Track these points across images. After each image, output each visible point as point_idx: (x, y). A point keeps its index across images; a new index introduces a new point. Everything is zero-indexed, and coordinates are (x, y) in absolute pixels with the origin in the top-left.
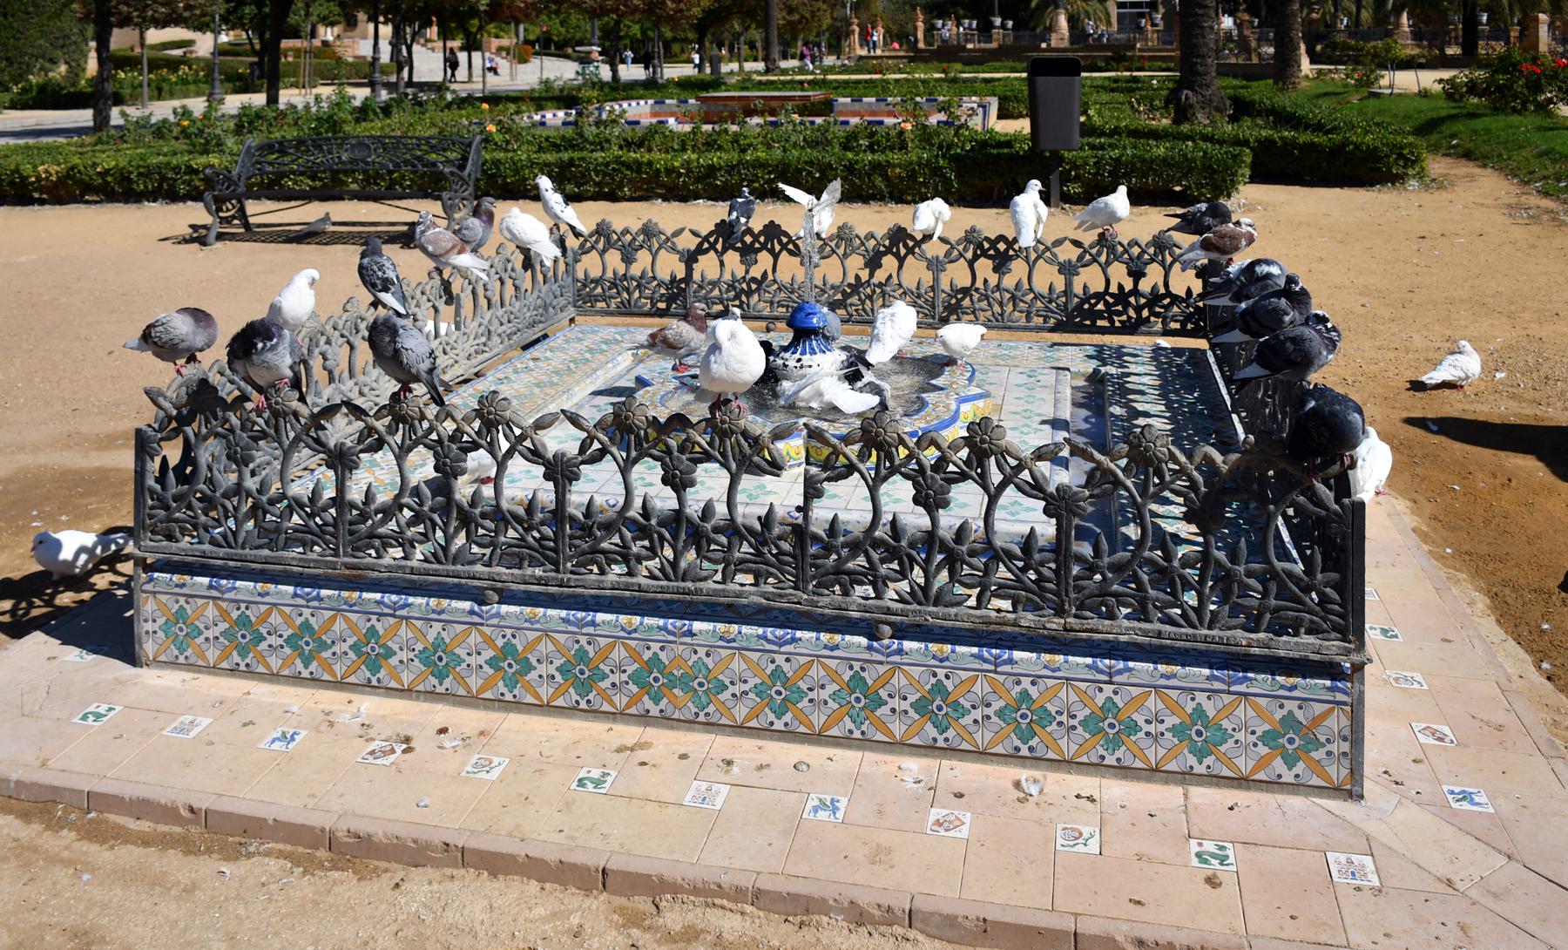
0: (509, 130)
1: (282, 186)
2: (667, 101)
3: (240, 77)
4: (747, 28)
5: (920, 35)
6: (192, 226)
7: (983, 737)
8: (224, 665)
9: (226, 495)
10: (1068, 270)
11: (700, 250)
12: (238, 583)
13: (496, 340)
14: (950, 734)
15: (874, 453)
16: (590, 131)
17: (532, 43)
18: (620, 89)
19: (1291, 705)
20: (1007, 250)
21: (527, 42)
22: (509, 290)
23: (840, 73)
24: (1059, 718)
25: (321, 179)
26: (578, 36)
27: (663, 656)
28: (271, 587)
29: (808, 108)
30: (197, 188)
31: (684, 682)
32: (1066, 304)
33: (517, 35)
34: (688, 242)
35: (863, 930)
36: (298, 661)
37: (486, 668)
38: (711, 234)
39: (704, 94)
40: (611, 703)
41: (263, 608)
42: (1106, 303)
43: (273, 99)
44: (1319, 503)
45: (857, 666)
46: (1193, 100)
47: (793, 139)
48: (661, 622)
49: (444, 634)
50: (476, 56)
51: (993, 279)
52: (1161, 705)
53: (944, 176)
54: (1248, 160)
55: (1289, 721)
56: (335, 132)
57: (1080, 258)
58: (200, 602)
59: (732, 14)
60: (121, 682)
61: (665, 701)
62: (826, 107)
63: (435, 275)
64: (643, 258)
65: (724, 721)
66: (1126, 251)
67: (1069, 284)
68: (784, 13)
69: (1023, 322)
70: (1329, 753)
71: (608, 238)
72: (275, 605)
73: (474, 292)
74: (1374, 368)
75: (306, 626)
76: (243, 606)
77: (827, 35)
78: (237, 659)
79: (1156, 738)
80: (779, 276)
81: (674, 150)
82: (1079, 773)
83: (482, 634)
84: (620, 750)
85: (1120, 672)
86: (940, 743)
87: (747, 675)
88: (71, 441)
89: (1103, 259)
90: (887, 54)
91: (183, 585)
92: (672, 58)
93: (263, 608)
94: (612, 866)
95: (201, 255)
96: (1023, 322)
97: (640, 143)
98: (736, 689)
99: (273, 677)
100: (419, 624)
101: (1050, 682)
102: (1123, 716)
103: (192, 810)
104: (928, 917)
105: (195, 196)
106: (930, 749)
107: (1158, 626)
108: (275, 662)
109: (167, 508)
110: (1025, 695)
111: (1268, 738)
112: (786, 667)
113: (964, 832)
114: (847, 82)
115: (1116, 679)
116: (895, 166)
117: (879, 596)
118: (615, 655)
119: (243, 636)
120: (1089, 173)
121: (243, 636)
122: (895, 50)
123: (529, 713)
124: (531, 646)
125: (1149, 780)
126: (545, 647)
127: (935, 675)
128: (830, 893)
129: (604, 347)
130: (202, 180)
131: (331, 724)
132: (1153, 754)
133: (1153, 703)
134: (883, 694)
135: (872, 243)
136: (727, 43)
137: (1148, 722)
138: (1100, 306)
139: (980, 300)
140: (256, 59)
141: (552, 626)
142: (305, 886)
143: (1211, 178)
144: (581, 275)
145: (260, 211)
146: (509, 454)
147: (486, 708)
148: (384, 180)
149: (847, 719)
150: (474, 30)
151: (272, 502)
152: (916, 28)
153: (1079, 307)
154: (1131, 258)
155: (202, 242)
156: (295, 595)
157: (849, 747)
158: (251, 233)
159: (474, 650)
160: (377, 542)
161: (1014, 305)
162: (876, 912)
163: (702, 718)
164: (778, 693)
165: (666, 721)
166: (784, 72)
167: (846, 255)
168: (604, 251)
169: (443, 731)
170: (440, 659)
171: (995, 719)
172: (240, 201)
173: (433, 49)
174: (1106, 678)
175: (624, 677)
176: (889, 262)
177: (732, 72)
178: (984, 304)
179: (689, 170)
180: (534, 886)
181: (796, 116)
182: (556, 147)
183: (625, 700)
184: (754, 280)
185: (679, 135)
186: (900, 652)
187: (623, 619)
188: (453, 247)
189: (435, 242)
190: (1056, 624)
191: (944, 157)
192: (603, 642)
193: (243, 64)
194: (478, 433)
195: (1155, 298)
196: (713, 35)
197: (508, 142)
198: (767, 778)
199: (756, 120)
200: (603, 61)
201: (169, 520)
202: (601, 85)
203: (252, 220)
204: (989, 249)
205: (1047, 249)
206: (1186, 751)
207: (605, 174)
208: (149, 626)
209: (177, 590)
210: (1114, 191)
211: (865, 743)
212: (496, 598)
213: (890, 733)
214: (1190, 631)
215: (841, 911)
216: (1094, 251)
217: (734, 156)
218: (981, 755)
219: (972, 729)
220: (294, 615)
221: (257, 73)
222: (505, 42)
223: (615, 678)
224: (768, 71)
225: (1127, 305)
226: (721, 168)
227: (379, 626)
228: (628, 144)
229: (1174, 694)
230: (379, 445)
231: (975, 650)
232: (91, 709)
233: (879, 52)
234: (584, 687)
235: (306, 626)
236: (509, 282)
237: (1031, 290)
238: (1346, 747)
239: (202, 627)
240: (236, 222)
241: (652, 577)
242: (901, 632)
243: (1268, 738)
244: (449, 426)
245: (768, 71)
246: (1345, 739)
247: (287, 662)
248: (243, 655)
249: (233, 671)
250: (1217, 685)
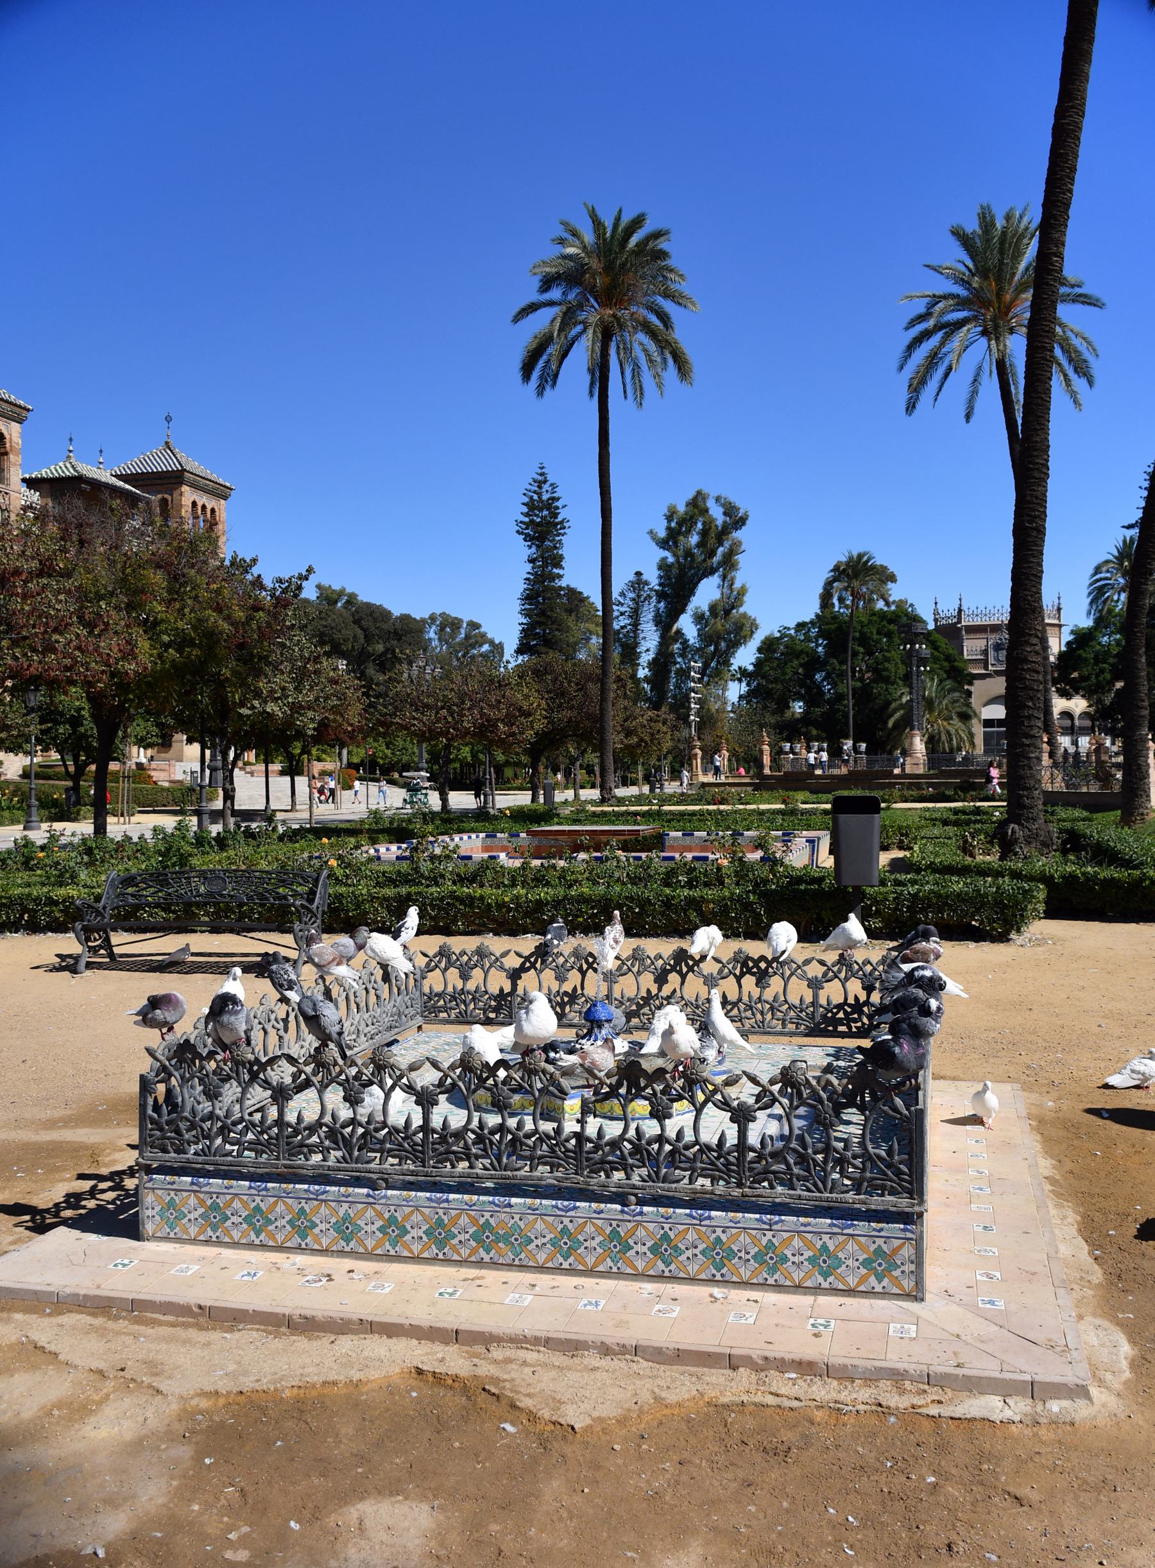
0: (349, 865)
1: (137, 918)
2: (499, 835)
3: (55, 804)
4: (583, 752)
5: (766, 760)
6: (57, 955)
7: (693, 1268)
8: (202, 1238)
9: (203, 1120)
10: (815, 985)
11: (522, 969)
12: (211, 1181)
13: (363, 1038)
14: (673, 1267)
15: (625, 1083)
16: (425, 867)
17: (355, 767)
18: (450, 821)
19: (880, 1241)
20: (767, 968)
21: (350, 765)
22: (372, 999)
23: (678, 803)
25: (174, 912)
26: (405, 758)
27: (492, 1221)
28: (234, 1183)
29: (632, 843)
30: (57, 919)
31: (505, 1238)
32: (813, 1013)
33: (341, 760)
34: (513, 962)
35: (608, 1358)
36: (252, 1233)
37: (378, 1233)
38: (531, 955)
39: (536, 828)
40: (459, 1254)
41: (228, 1197)
42: (845, 1012)
43: (100, 829)
44: (895, 1109)
45: (614, 1223)
46: (1020, 834)
47: (617, 875)
48: (491, 1199)
49: (350, 1211)
50: (302, 782)
51: (756, 992)
52: (801, 1244)
53: (754, 911)
54: (1042, 896)
55: (879, 1252)
56: (181, 866)
57: (825, 974)
58: (185, 1194)
59: (567, 737)
60: (135, 1249)
61: (493, 1251)
62: (657, 842)
63: (320, 981)
64: (477, 973)
65: (531, 1264)
66: (861, 969)
67: (816, 996)
68: (622, 736)
69: (779, 1028)
70: (903, 1272)
71: (449, 959)
72: (236, 1194)
73: (347, 998)
74: (1082, 1074)
75: (258, 1208)
76: (215, 1196)
77: (670, 757)
78: (210, 1233)
79: (798, 1265)
80: (585, 992)
81: (505, 886)
82: (751, 1290)
83: (375, 1210)
84: (465, 1280)
85: (776, 1223)
86: (667, 1274)
87: (545, 1232)
88: (18, 1123)
89: (842, 975)
90: (730, 780)
91: (173, 1183)
92: (504, 784)
93: (228, 1197)
94: (462, 1327)
95: (73, 982)
96: (779, 1028)
97: (472, 878)
98: (539, 1242)
99: (235, 1245)
100: (333, 1204)
101: (734, 1231)
102: (778, 1252)
103: (200, 1307)
104: (645, 1348)
105: (58, 927)
106: (660, 1278)
107: (799, 1192)
108: (236, 1235)
109: (161, 1129)
110: (718, 1239)
111: (866, 1263)
112: (570, 1226)
113: (675, 1315)
114: (682, 814)
115: (774, 1227)
116: (708, 901)
117: (628, 1178)
118: (461, 1222)
119: (215, 1217)
120: (889, 909)
121: (215, 1217)
122: (740, 776)
123: (405, 1262)
124: (407, 1217)
125: (794, 1293)
126: (416, 1218)
127: (663, 1228)
128: (589, 1339)
129: (446, 1047)
130: (61, 911)
131: (278, 1269)
132: (797, 1276)
133: (797, 1242)
134: (631, 1242)
135: (661, 962)
136: (562, 767)
137: (794, 1255)
139: (745, 1010)
140: (70, 784)
141: (421, 1203)
142: (277, 1344)
143: (1003, 913)
144: (426, 990)
145: (123, 942)
146: (393, 1088)
147: (378, 1261)
148: (234, 913)
149: (608, 1260)
150: (297, 751)
151: (235, 1124)
152: (761, 752)
153: (824, 1016)
154: (864, 975)
155: (73, 970)
156: (250, 1187)
157: (610, 1278)
158: (116, 963)
159: (369, 1221)
160: (305, 1150)
161: (773, 1014)
162: (616, 1348)
163: (517, 1262)
164: (566, 1243)
165: (494, 1265)
166: (620, 801)
167: (639, 973)
168: (446, 969)
169: (351, 1271)
170: (347, 1228)
171: (700, 1256)
172: (106, 932)
173: (252, 773)
174: (768, 1227)
175: (467, 1236)
176: (674, 978)
177: (566, 802)
178: (749, 1013)
179: (518, 905)
180: (415, 1342)
181: (620, 852)
182: (392, 882)
183: (468, 1251)
184: (566, 993)
185: (510, 870)
186: (641, 1213)
187: (467, 1197)
188: (333, 960)
189: (320, 955)
190: (737, 1192)
191: (754, 893)
192: (453, 1212)
193: (59, 789)
194: (372, 1074)
196: (548, 759)
197: (347, 877)
198: (556, 1292)
199: (582, 856)
200: (431, 788)
201: (164, 1138)
202: (428, 817)
203: (116, 950)
205: (799, 967)
207: (440, 909)
208: (149, 1213)
209: (169, 1186)
210: (846, 920)
211: (620, 1275)
212: (384, 1185)
213: (635, 1268)
214: (818, 1194)
215: (595, 1348)
216: (835, 969)
217: (561, 892)
218: (692, 1280)
219: (686, 1263)
220: (249, 1201)
221: (73, 799)
222: (329, 766)
223: (461, 1237)
224: (603, 801)
225: (861, 1013)
226: (548, 903)
227: (307, 1207)
228: (461, 880)
229: (809, 1236)
230: (307, 1084)
231: (688, 1211)
232: (119, 1261)
233: (723, 779)
234: (441, 1244)
235: (258, 1208)
236: (372, 992)
237: (786, 1001)
238: (913, 1267)
239: (186, 1212)
240: (102, 952)
241: (485, 1169)
242: (641, 1202)
243: (866, 1263)
244: (353, 1071)
245: (603, 801)
246: (912, 1262)
247: (244, 1234)
248: (214, 1230)
249: (207, 1242)
250: (836, 1230)
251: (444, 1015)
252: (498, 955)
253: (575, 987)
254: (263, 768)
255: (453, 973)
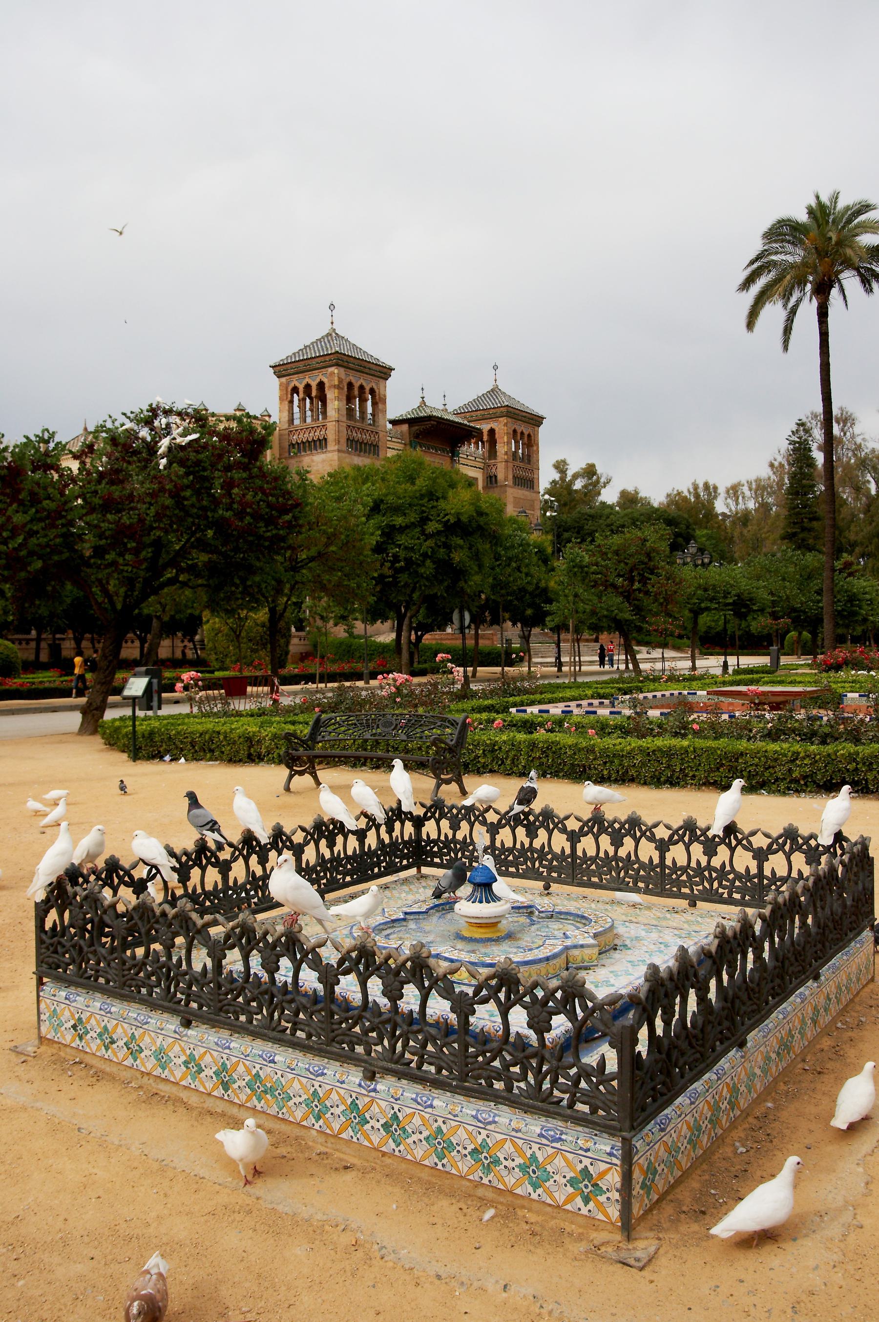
14: (402, 1147)
24: (458, 1148)
31: (270, 1091)
42: (688, 875)
52: (512, 1149)
64: (723, 852)
70: (608, 1199)
111: (572, 1182)
127: (393, 1109)
134: (367, 1115)
138: (684, 878)
171: (424, 1142)
195: (722, 872)
204: (803, 844)
206: (526, 1182)
209: (159, 1031)
219: (413, 1146)
243: (572, 1182)
251: (437, 860)
252: (746, 832)
253: (630, 853)
254: (481, 642)
255: (445, 824)
